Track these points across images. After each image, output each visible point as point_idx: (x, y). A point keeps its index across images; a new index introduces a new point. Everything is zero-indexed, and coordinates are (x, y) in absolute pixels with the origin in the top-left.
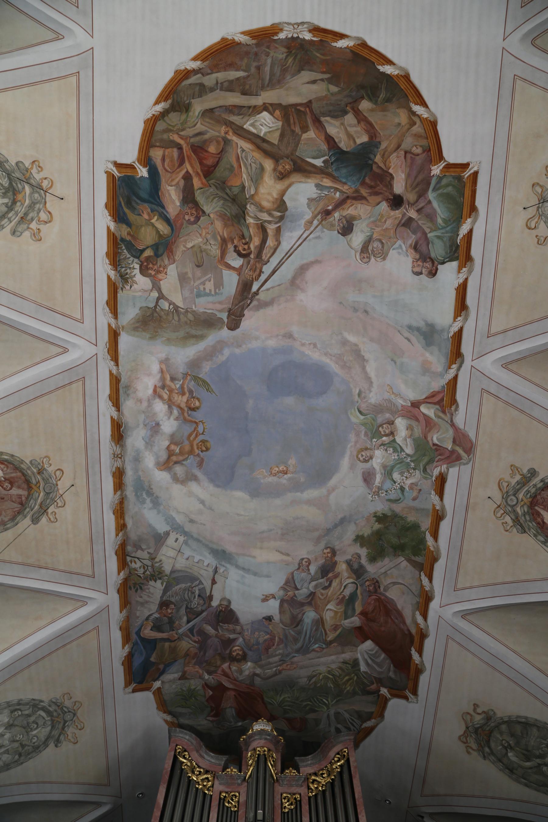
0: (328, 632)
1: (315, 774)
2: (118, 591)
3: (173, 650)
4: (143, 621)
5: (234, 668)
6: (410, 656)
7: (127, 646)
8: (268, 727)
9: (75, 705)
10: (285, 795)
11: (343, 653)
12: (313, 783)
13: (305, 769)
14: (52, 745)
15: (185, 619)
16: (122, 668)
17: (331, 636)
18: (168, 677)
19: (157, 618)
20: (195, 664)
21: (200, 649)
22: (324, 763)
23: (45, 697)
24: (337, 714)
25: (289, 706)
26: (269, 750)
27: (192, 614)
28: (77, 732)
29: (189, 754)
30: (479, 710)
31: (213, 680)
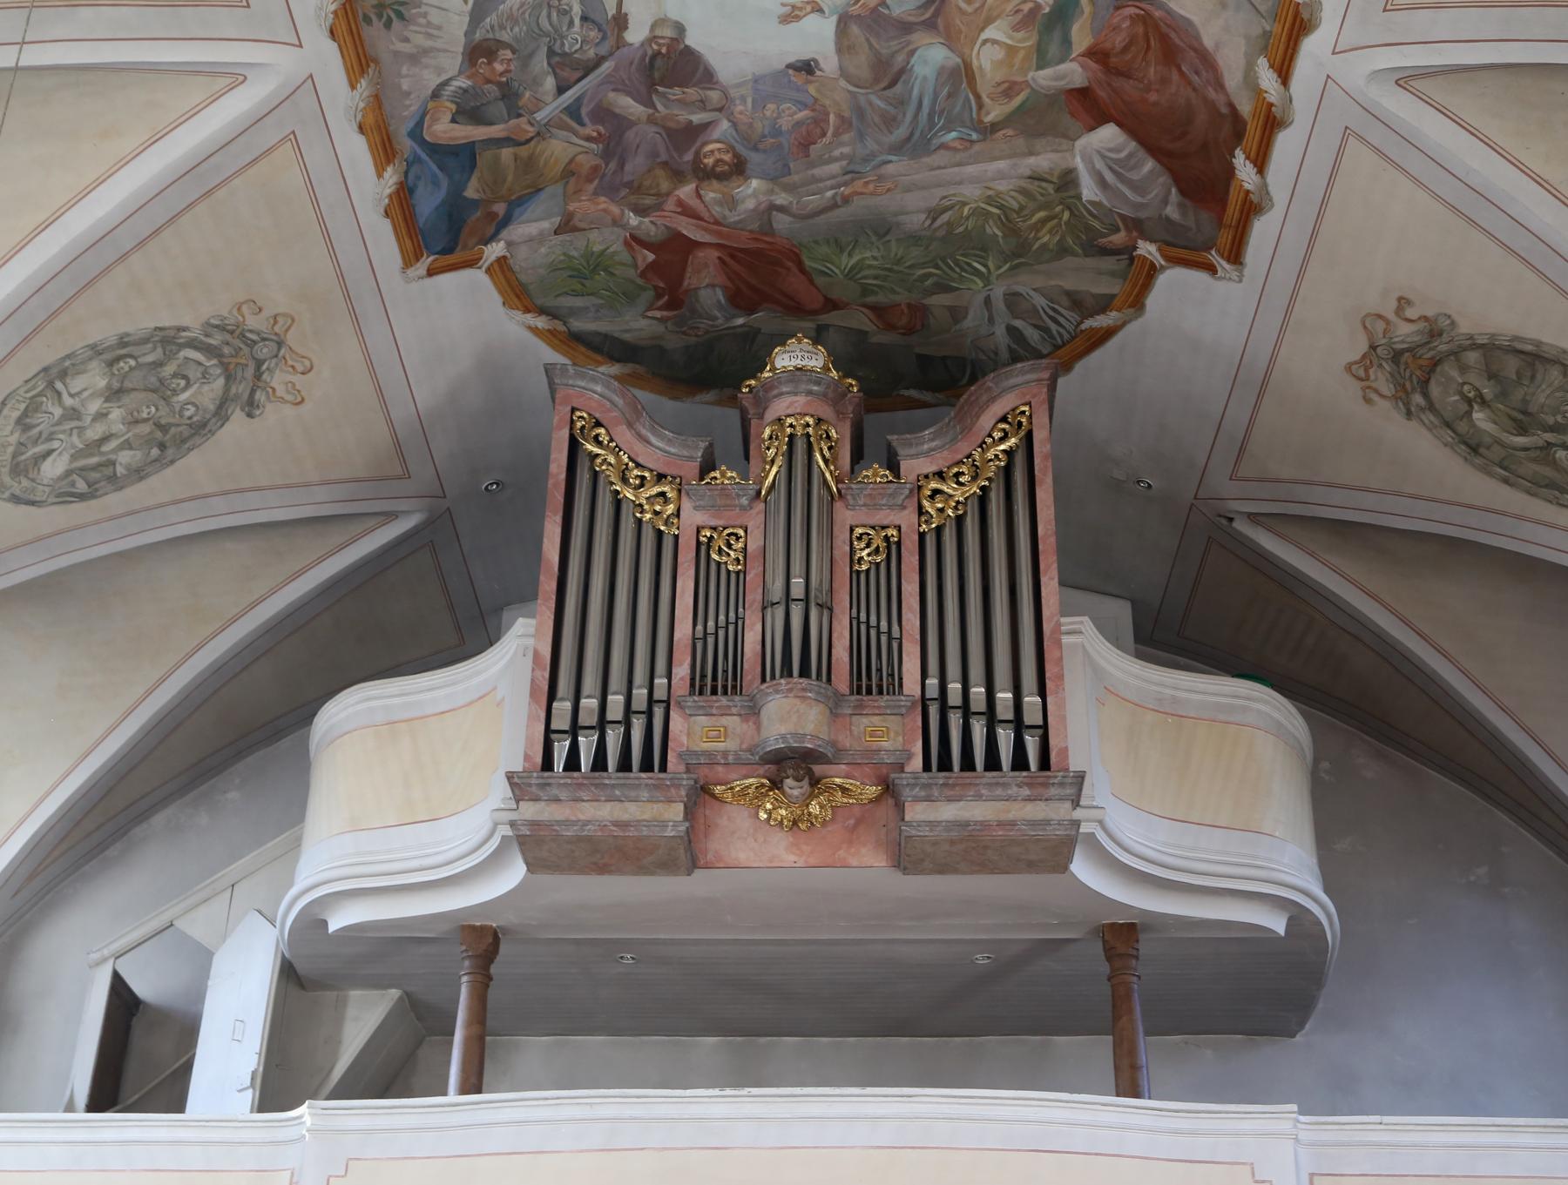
0: (986, 100)
1: (940, 475)
2: (332, 32)
3: (528, 165)
4: (425, 104)
5: (710, 196)
6: (1230, 171)
7: (390, 169)
8: (815, 360)
9: (276, 322)
10: (859, 531)
11: (1031, 154)
12: (932, 497)
13: (914, 462)
14: (238, 416)
15: (550, 83)
16: (387, 226)
17: (994, 113)
18: (521, 230)
19: (465, 91)
20: (596, 193)
21: (607, 155)
22: (964, 447)
23: (191, 318)
24: (1012, 299)
25: (876, 278)
26: (819, 421)
27: (570, 69)
28: (296, 378)
29: (608, 433)
30: (1411, 313)
31: (653, 228)
